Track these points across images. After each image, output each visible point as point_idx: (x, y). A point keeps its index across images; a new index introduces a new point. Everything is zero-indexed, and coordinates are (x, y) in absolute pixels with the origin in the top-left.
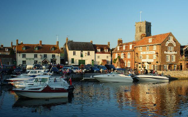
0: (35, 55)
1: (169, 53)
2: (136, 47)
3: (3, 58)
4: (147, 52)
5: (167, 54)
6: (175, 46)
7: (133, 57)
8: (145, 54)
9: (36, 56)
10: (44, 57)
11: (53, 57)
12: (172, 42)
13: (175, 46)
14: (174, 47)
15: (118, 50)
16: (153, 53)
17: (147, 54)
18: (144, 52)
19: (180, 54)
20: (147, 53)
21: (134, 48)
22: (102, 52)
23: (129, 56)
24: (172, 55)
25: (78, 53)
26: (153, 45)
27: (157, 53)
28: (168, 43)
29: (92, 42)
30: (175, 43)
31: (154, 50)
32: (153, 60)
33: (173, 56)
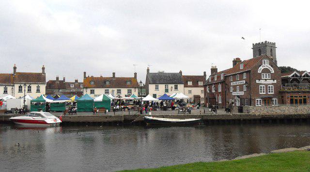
0: (106, 91)
1: (262, 82)
3: (157, 103)
5: (261, 84)
6: (273, 72)
9: (107, 92)
10: (118, 92)
11: (128, 92)
13: (273, 72)
17: (237, 85)
19: (281, 83)
21: (226, 77)
22: (195, 85)
25: (162, 87)
28: (261, 68)
29: (181, 72)
33: (271, 86)
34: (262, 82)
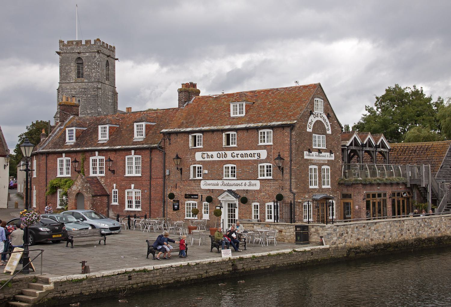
1: (314, 156)
2: (170, 134)
4: (229, 153)
7: (157, 172)
8: (215, 158)
12: (321, 120)
13: (329, 132)
14: (327, 136)
15: (70, 141)
16: (256, 157)
18: (215, 153)
20: (229, 158)
23: (133, 166)
24: (323, 164)
26: (257, 129)
27: (280, 158)
28: (312, 119)
30: (329, 124)
31: (265, 147)
32: (258, 182)
34: (314, 156)
